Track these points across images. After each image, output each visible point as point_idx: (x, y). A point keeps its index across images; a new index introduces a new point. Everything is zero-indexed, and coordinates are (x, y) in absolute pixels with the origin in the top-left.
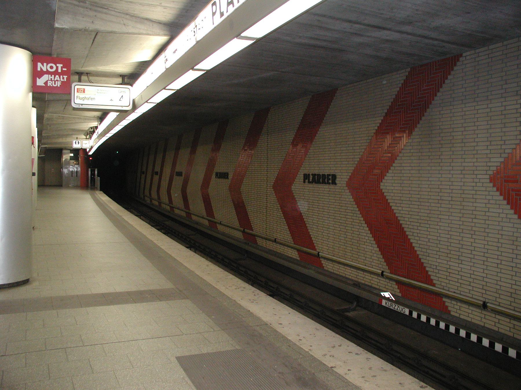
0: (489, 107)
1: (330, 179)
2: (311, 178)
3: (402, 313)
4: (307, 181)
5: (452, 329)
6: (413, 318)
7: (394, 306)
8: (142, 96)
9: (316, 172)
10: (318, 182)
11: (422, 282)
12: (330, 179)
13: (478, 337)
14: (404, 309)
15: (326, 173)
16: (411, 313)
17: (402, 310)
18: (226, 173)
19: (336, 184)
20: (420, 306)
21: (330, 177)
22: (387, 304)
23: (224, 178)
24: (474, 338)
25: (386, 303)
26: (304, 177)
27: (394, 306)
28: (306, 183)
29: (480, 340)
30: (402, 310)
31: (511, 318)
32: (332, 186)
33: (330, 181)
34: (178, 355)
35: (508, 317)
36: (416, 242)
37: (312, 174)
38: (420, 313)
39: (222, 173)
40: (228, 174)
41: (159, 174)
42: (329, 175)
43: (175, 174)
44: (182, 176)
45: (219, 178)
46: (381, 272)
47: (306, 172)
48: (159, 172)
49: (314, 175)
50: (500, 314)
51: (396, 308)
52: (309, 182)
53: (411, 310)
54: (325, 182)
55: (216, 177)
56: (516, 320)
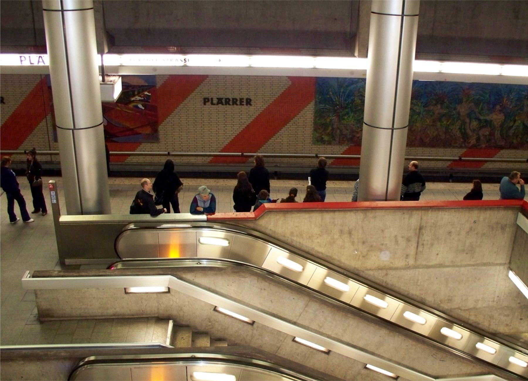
2: (215, 101)
4: (209, 103)
19: (251, 105)
33: (245, 103)
52: (212, 104)
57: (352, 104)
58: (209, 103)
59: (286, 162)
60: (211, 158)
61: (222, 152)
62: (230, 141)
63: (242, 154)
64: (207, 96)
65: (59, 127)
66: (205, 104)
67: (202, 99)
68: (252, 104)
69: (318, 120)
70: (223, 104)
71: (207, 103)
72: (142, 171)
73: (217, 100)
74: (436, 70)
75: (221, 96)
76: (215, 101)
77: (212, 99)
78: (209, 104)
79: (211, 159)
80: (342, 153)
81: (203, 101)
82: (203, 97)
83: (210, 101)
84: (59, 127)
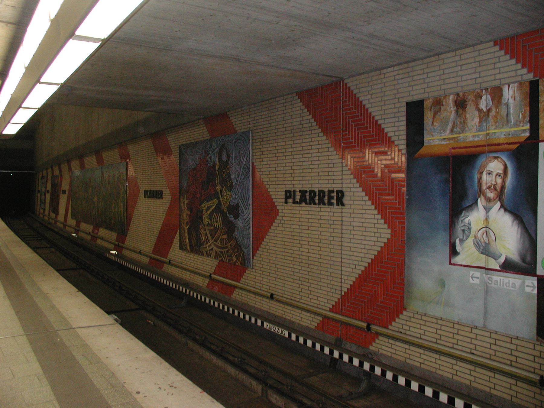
0: (397, 109)
1: (333, 198)
2: (298, 198)
3: (282, 336)
4: (291, 201)
5: (415, 386)
6: (441, 402)
7: (274, 328)
8: (5, 121)
9: (307, 187)
10: (312, 201)
11: (233, 280)
12: (333, 198)
13: (382, 370)
14: (283, 332)
15: (326, 188)
16: (290, 335)
17: (282, 332)
18: (159, 191)
19: (343, 205)
20: (354, 348)
21: (334, 194)
22: (268, 326)
23: (157, 198)
24: (429, 392)
25: (267, 326)
26: (286, 195)
27: (274, 328)
28: (289, 204)
29: (436, 394)
30: (282, 332)
31: (475, 365)
32: (336, 208)
33: (334, 201)
35: (479, 366)
36: (327, 262)
37: (300, 191)
38: (245, 313)
39: (154, 191)
40: (162, 192)
41: (50, 192)
42: (331, 192)
43: (61, 192)
44: (65, 194)
45: (148, 197)
46: (169, 261)
47: (289, 187)
48: (61, 193)
49: (303, 192)
50: (472, 364)
51: (277, 330)
52: (295, 202)
53: (372, 364)
54: (307, 202)
55: (145, 197)
56: (492, 371)
70: (306, 203)
78: (291, 201)
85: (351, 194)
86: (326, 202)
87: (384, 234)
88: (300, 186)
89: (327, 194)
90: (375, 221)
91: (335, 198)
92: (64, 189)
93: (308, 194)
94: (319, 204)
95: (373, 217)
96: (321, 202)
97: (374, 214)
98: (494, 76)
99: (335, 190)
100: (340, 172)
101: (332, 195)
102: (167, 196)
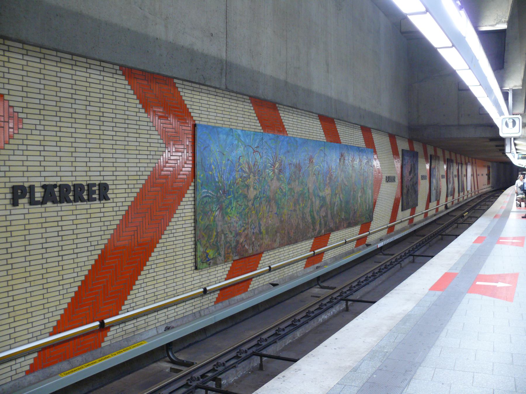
2: (39, 195)
4: (25, 200)
15: (83, 180)
19: (106, 198)
33: (96, 196)
34: (190, 264)
37: (44, 187)
52: (32, 202)
57: (234, 186)
58: (25, 200)
59: (476, 197)
60: (30, 359)
61: (60, 332)
62: (72, 298)
63: (102, 324)
64: (18, 181)
65: (439, 48)
66: (15, 203)
67: (7, 190)
68: (110, 196)
69: (202, 220)
70: (54, 202)
71: (21, 201)
72: (428, 245)
73: (43, 190)
74: (486, 75)
75: (51, 181)
76: (39, 195)
77: (32, 188)
78: (23, 201)
79: (32, 361)
80: (225, 276)
81: (9, 196)
82: (10, 185)
83: (28, 196)
84: (439, 48)
85: (114, 187)
86: (86, 197)
87: (98, 64)
88: (42, 179)
89: (86, 188)
90: (126, 91)
91: (97, 192)
92: (425, 181)
93: (57, 190)
94: (75, 201)
95: (134, 105)
96: (78, 198)
97: (125, 85)
98: (43, 305)
99: (97, 183)
100: (5, 103)
101: (94, 188)
102: (420, 177)
